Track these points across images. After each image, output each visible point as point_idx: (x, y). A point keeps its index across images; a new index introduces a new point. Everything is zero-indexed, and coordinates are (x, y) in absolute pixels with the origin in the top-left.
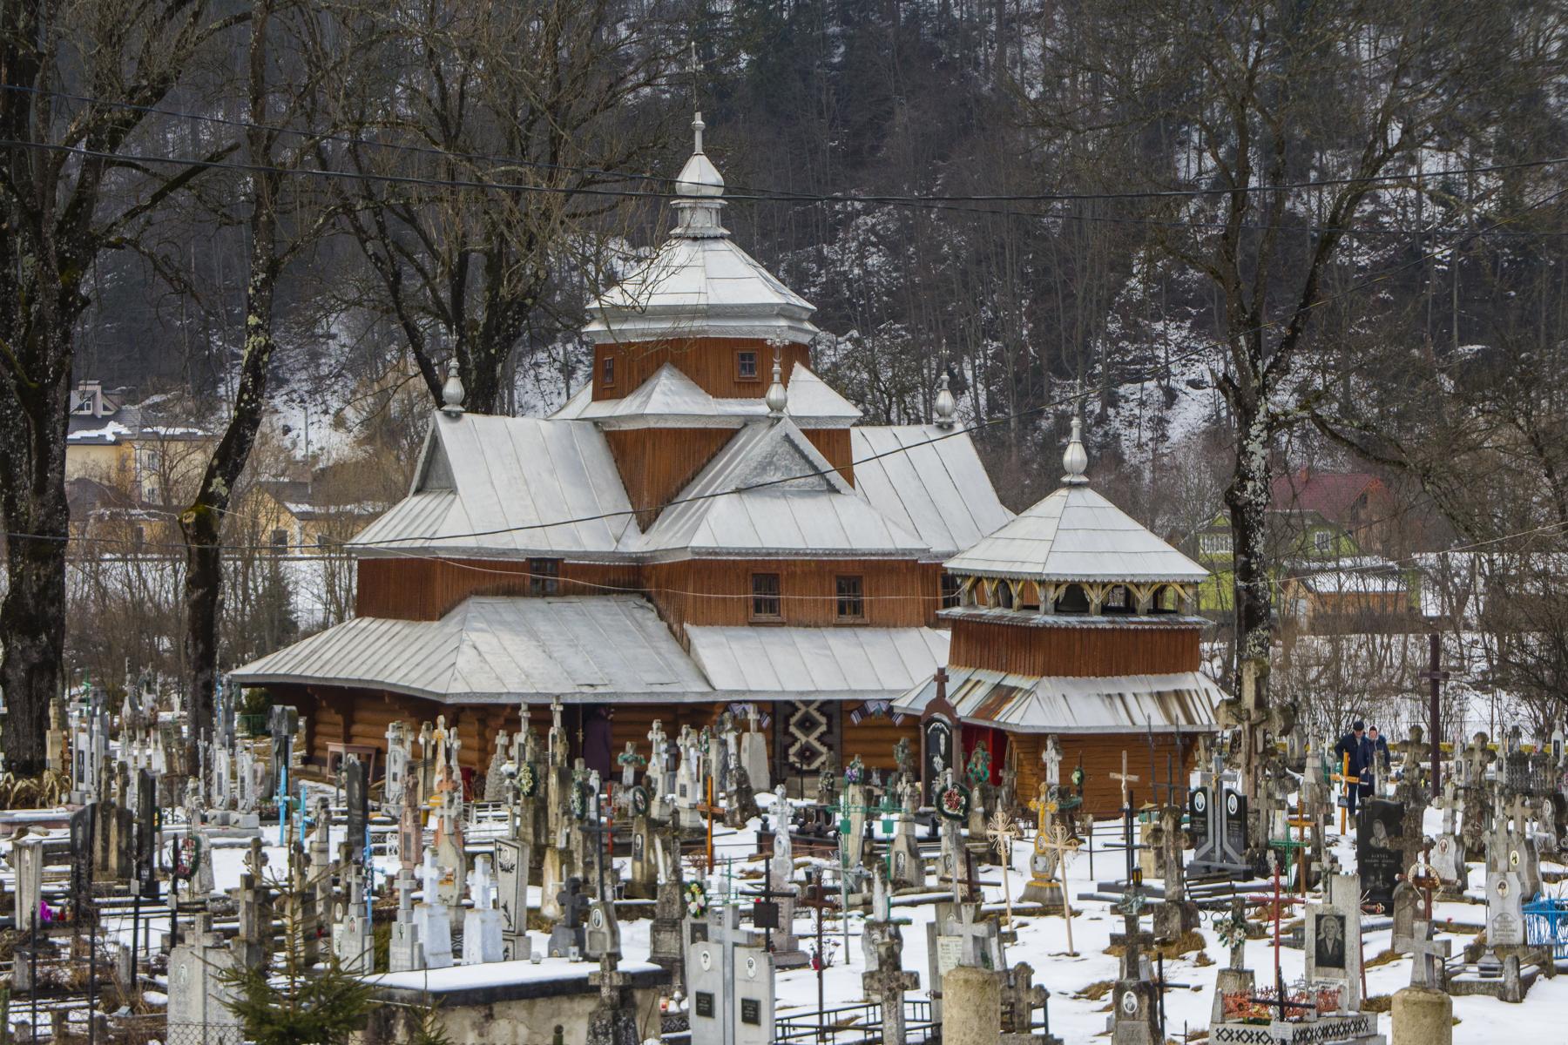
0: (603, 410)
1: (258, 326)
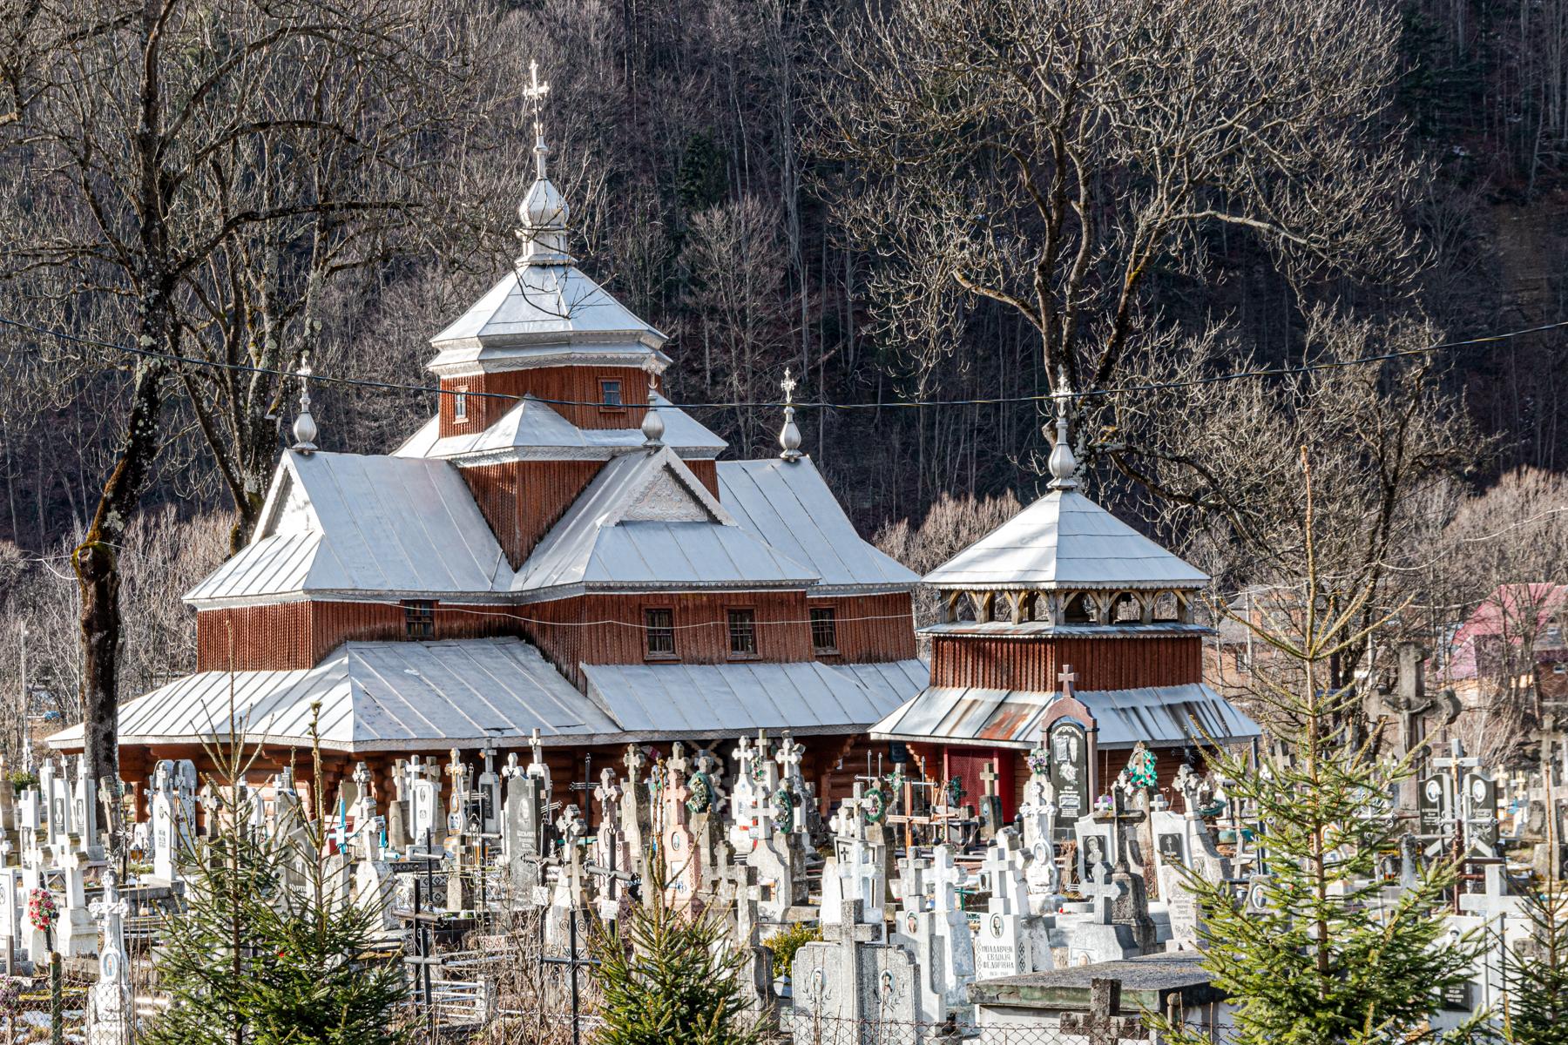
0: (460, 446)
1: (152, 347)
